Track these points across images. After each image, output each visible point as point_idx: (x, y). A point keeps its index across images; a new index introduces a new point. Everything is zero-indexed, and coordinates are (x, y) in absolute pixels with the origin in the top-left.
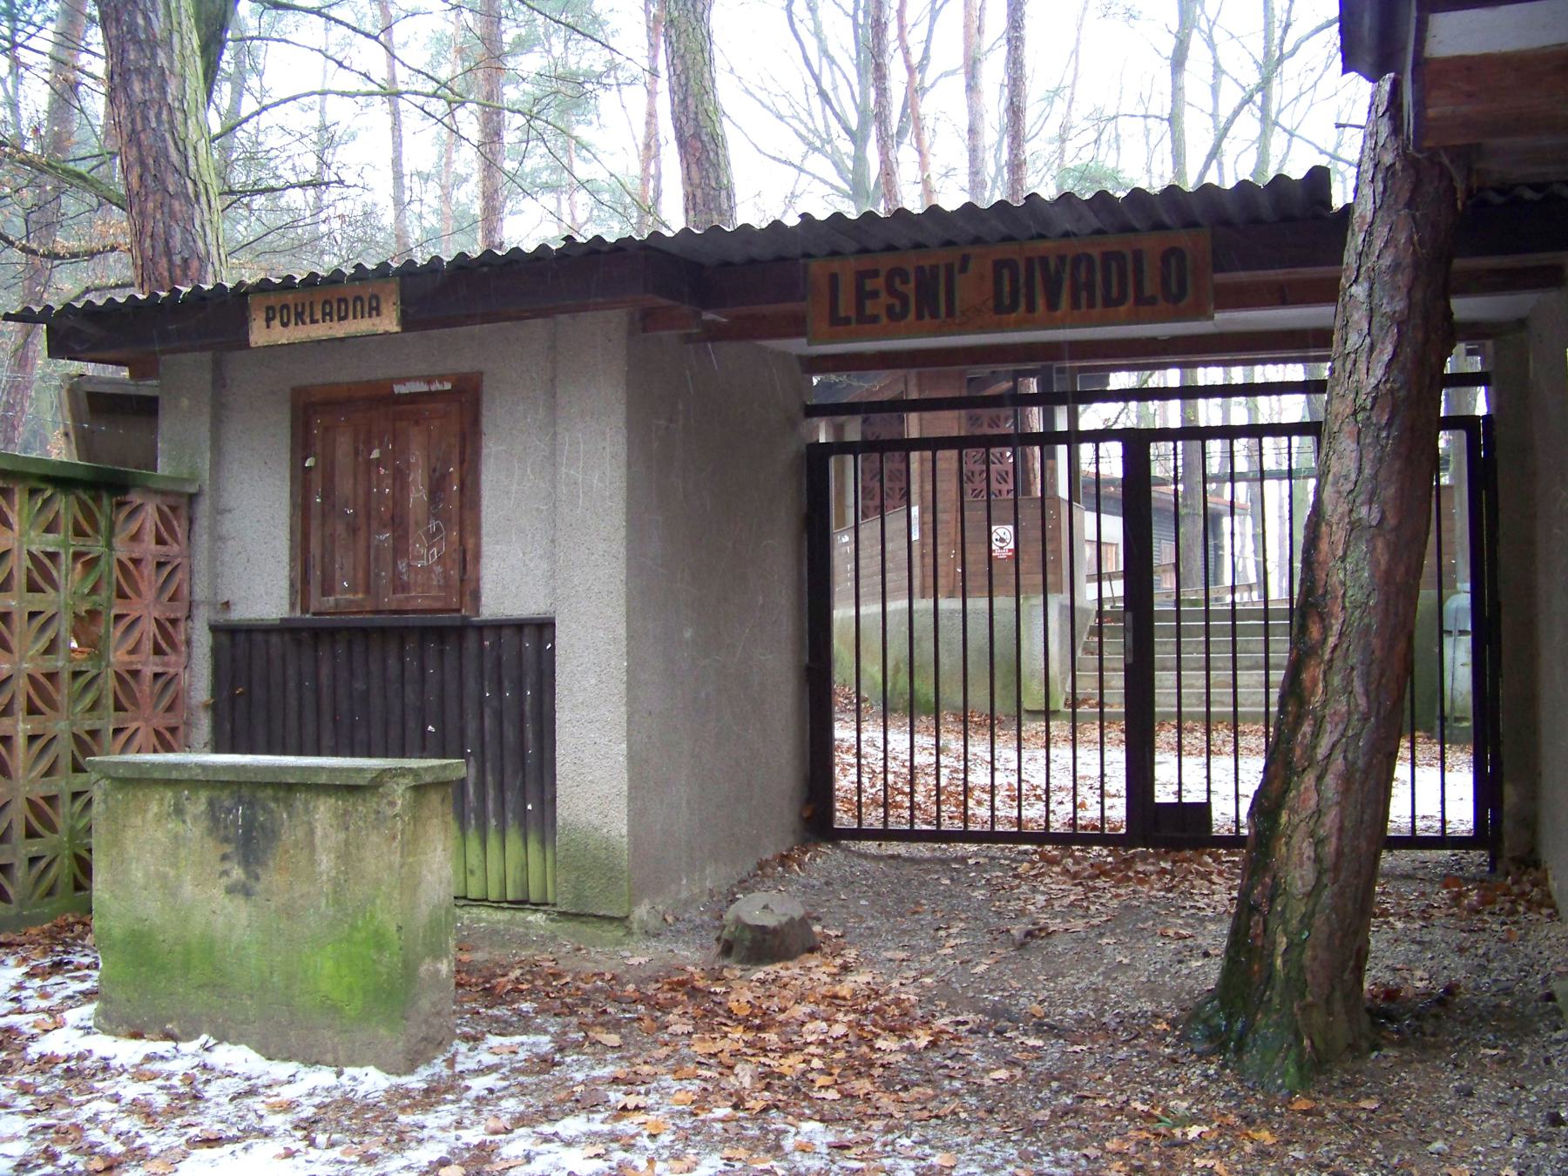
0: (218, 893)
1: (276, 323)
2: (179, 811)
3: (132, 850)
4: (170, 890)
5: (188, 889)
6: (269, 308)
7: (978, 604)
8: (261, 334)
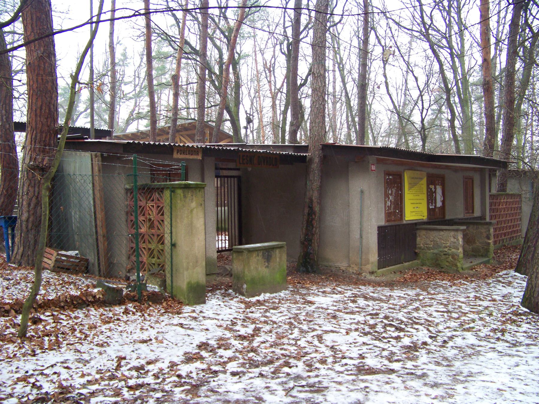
0: (264, 268)
1: (179, 153)
2: (258, 255)
3: (251, 264)
4: (256, 269)
5: (260, 269)
6: (178, 150)
7: (219, 208)
8: (176, 155)
